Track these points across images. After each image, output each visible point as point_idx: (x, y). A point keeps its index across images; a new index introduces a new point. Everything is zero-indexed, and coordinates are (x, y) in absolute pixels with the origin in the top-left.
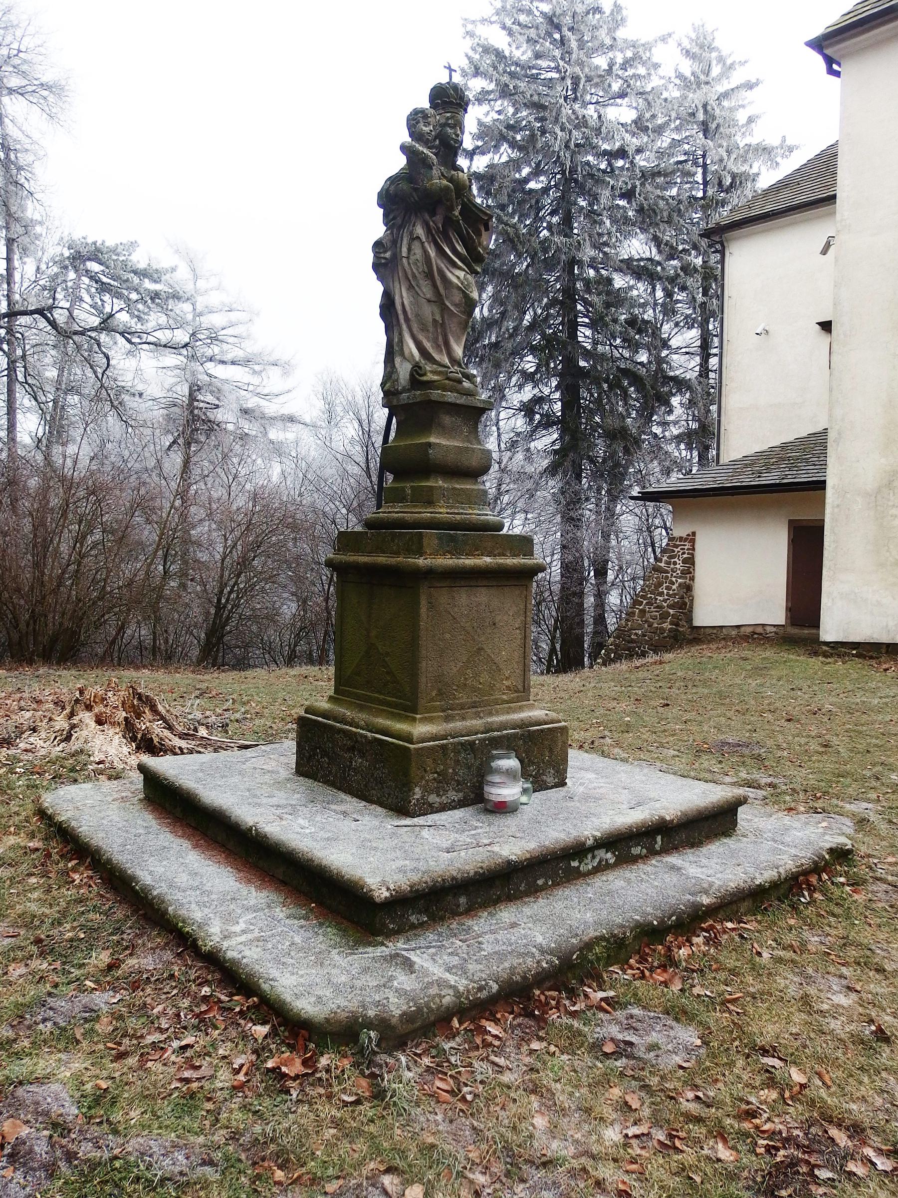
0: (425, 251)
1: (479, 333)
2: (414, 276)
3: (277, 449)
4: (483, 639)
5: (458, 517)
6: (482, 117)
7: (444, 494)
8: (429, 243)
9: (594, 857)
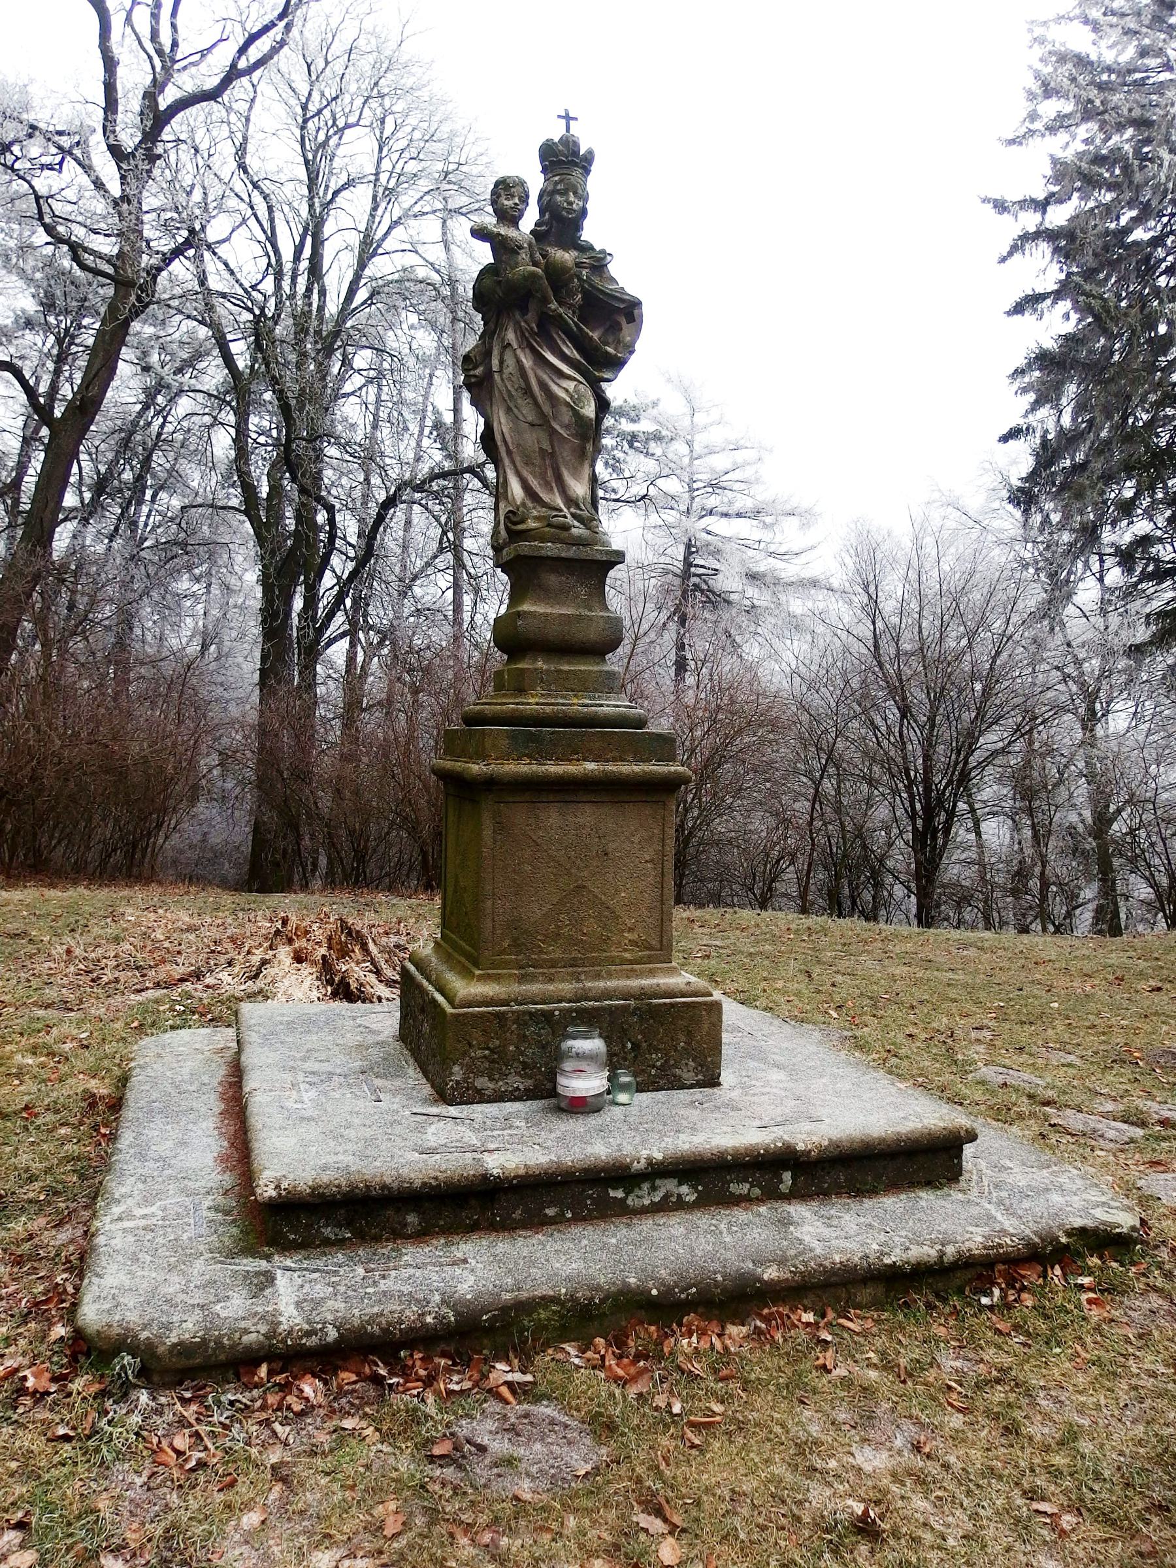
1: (1054, 451)
3: (796, 626)
4: (586, 874)
5: (548, 709)
6: (1060, 154)
9: (654, 1188)
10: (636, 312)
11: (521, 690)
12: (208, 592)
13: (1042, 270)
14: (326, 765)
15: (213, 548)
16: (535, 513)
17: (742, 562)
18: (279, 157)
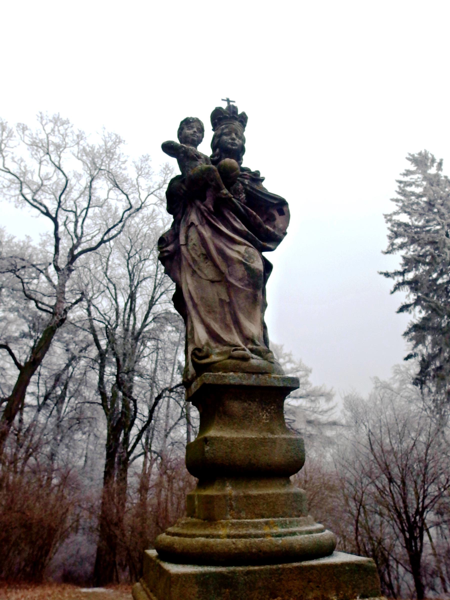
0: (200, 234)
2: (194, 260)
3: (330, 442)
6: (406, 256)
7: (231, 506)
8: (203, 226)
10: (285, 209)
11: (210, 519)
12: (88, 439)
13: (406, 296)
14: (128, 519)
15: (92, 420)
16: (217, 351)
17: (305, 416)
18: (120, 271)
